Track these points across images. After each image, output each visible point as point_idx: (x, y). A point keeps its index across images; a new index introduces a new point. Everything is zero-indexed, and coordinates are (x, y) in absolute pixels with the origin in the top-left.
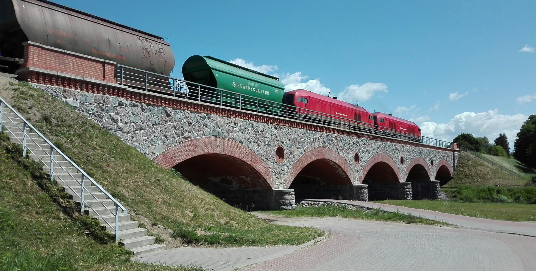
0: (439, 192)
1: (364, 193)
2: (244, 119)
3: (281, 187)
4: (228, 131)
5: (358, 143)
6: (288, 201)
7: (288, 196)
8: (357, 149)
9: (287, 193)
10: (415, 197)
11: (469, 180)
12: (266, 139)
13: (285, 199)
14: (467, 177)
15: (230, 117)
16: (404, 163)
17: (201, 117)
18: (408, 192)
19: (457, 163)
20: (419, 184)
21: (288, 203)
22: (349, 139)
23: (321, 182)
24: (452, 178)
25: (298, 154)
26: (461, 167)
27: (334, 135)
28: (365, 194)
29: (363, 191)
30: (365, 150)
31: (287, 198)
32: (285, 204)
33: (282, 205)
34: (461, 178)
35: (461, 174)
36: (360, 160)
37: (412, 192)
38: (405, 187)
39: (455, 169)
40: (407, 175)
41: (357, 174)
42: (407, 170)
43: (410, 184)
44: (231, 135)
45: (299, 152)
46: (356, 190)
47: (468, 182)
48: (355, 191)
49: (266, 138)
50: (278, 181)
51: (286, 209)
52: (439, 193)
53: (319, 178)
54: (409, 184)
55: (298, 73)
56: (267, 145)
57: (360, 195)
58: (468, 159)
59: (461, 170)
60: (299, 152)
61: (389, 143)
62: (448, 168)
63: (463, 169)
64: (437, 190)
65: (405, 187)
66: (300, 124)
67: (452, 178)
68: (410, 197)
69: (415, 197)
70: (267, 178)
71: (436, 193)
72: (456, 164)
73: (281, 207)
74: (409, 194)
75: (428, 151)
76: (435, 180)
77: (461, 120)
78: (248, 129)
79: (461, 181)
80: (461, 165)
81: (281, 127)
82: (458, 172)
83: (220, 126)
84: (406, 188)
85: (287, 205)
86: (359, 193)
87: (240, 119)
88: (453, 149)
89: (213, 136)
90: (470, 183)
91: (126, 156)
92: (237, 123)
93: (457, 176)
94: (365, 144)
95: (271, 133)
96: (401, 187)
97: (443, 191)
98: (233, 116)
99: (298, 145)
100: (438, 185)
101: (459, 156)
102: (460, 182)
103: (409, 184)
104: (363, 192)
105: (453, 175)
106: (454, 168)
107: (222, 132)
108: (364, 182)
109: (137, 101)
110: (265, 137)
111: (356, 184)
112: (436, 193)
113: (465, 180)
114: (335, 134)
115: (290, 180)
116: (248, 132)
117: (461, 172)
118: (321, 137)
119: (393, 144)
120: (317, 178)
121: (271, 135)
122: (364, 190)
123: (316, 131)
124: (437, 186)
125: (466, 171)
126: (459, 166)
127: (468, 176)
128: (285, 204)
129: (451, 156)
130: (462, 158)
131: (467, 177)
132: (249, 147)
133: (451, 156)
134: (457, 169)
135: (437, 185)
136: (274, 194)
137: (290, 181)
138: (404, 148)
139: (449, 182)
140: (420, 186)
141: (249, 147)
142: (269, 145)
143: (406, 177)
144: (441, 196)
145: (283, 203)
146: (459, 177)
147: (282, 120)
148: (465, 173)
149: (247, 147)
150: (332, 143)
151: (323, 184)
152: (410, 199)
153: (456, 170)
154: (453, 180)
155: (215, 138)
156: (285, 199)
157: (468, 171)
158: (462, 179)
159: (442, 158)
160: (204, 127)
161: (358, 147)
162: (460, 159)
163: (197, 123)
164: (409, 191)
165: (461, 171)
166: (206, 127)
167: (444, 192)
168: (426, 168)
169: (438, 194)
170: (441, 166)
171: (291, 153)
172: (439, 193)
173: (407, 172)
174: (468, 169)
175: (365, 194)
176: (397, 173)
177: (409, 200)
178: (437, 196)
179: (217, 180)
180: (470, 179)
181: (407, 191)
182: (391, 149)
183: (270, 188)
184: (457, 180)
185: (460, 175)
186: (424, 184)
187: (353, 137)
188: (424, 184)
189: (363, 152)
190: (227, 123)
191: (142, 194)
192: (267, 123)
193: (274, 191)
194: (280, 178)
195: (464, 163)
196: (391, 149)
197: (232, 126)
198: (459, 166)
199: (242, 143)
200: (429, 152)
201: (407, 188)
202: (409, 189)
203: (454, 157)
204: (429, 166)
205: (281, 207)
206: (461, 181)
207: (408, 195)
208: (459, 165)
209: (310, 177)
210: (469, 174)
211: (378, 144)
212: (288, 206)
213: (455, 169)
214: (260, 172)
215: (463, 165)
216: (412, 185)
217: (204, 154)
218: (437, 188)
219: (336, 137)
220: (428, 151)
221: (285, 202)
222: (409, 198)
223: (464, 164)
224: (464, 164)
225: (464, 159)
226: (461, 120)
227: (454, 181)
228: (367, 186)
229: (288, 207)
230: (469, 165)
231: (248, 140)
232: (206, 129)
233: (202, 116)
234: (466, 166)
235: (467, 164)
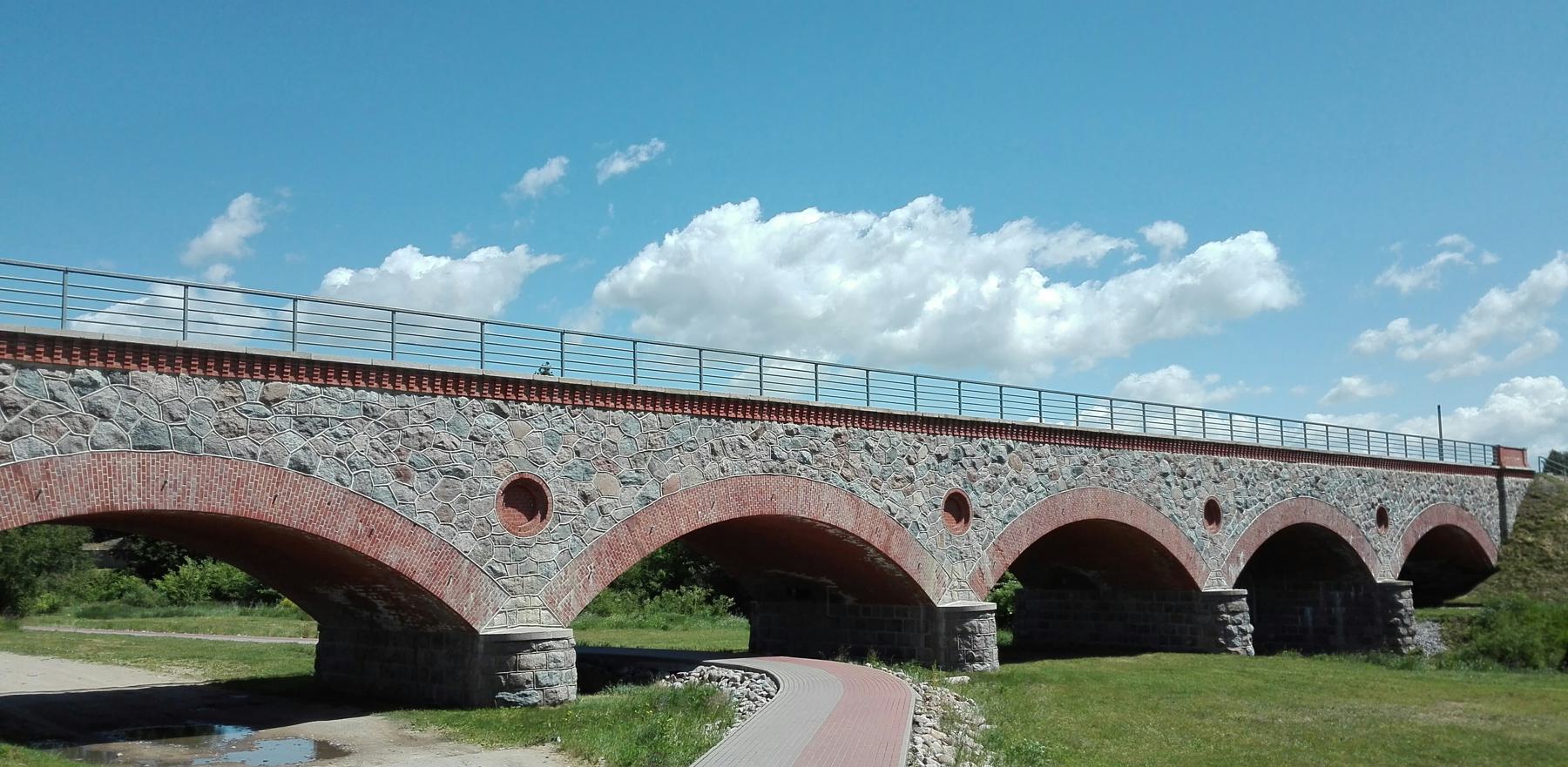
0: (1407, 621)
1: (974, 633)
2: (795, 423)
3: (527, 621)
4: (223, 427)
5: (965, 455)
6: (528, 675)
7: (528, 656)
8: (959, 478)
9: (1399, 588)
10: (1266, 645)
11: (1555, 575)
12: (440, 454)
13: (517, 667)
14: (1546, 565)
15: (238, 380)
16: (1223, 521)
17: (73, 384)
18: (1230, 627)
19: (1518, 516)
21: (528, 682)
22: (914, 442)
23: (840, 592)
24: (1496, 570)
25: (1411, 514)
26: (1531, 530)
27: (828, 432)
28: (977, 638)
29: (972, 626)
30: (1004, 480)
31: (524, 664)
32: (515, 686)
33: (503, 689)
34: (1526, 571)
35: (1526, 555)
36: (976, 516)
37: (1252, 622)
38: (1222, 607)
39: (1509, 537)
40: (1243, 565)
41: (959, 566)
42: (1241, 545)
43: (1244, 596)
44: (244, 442)
45: (631, 495)
46: (944, 624)
47: (1549, 586)
48: (942, 629)
49: (443, 448)
50: (508, 602)
51: (516, 704)
52: (1406, 626)
53: (830, 581)
54: (1240, 597)
56: (447, 473)
57: (958, 640)
58: (1560, 503)
59: (1530, 539)
60: (631, 495)
61: (1138, 454)
62: (1474, 536)
63: (1537, 536)
64: (1401, 616)
65: (1222, 607)
66: (1034, 431)
67: (1496, 570)
68: (1244, 645)
69: (1266, 645)
70: (450, 596)
71: (1396, 625)
72: (1511, 521)
73: (500, 695)
74: (1236, 632)
76: (1399, 579)
78: (341, 420)
79: (1525, 581)
80: (1532, 523)
81: (533, 407)
82: (1516, 548)
83: (177, 412)
84: (1223, 609)
85: (524, 688)
86: (956, 633)
87: (294, 386)
88: (1498, 467)
89: (144, 447)
90: (1556, 589)
92: (277, 400)
93: (1514, 560)
94: (1001, 460)
95: (471, 429)
96: (1206, 608)
97: (1431, 616)
98: (1012, 436)
99: (625, 470)
100: (1406, 599)
101: (1530, 489)
102: (1519, 585)
103: (1240, 597)
104: (970, 630)
105: (1499, 559)
106: (1504, 533)
107: (192, 434)
108: (1404, 575)
109: (208, 374)
110: (435, 446)
111: (953, 600)
112: (1396, 625)
113: (1539, 576)
114: (832, 427)
115: (582, 594)
116: (340, 429)
117: (1526, 547)
118: (755, 439)
119: (1159, 454)
120: (824, 580)
121: (472, 438)
122: (974, 622)
123: (728, 418)
124: (1401, 601)
125: (1548, 544)
126: (1524, 526)
127: (1550, 560)
128: (515, 686)
130: (1536, 497)
131: (1546, 565)
132: (344, 485)
134: (1513, 537)
135: (1401, 597)
136: (481, 647)
137: (1236, 571)
138: (1222, 469)
139: (1481, 586)
140: (1339, 601)
141: (344, 485)
142: (460, 474)
144: (1416, 637)
145: (507, 681)
146: (1520, 565)
147: (899, 418)
148: (1541, 549)
149: (336, 483)
150: (819, 460)
151: (849, 600)
152: (1238, 649)
153: (1512, 540)
154: (1497, 575)
155: (148, 456)
156: (517, 667)
157: (1553, 545)
158: (1527, 573)
159: (1435, 500)
160: (90, 417)
161: (961, 471)
162: (1531, 500)
163: (47, 406)
164: (1234, 624)
165: (1529, 544)
166: (101, 416)
167: (1436, 621)
168: (1350, 539)
169: (1402, 630)
170: (1431, 527)
171: (585, 498)
172: (1406, 626)
174: (1556, 535)
175: (977, 638)
176: (1182, 559)
177: (1237, 653)
178: (1402, 636)
179: (338, 596)
180: (1557, 572)
181: (1226, 623)
182: (1146, 474)
183: (1190, 584)
184: (1511, 575)
185: (1525, 558)
186: (1352, 594)
187: (935, 435)
188: (1352, 594)
189: (990, 488)
190: (219, 399)
192: (452, 396)
193: (482, 639)
194: (518, 589)
195: (1543, 515)
196: (1146, 474)
197: (248, 412)
198: (1524, 526)
199: (305, 470)
200: (1364, 481)
201: (1229, 612)
202: (1234, 613)
203: (1502, 496)
205: (500, 695)
206: (1525, 581)
207: (1231, 635)
208: (1523, 523)
209: (802, 576)
210: (1557, 554)
211: (1075, 457)
212: (528, 692)
213: (1509, 537)
214: (409, 573)
215: (1538, 523)
216: (1413, 588)
217: (87, 513)
218: (1401, 606)
219: (838, 436)
221: (513, 677)
222: (1235, 646)
223: (1542, 518)
224: (1542, 518)
225: (1544, 502)
227: (1499, 579)
228: (1245, 592)
229: (526, 695)
230: (1558, 524)
231: (341, 458)
232: (97, 425)
233: (76, 378)
234: (1549, 528)
235: (1553, 521)
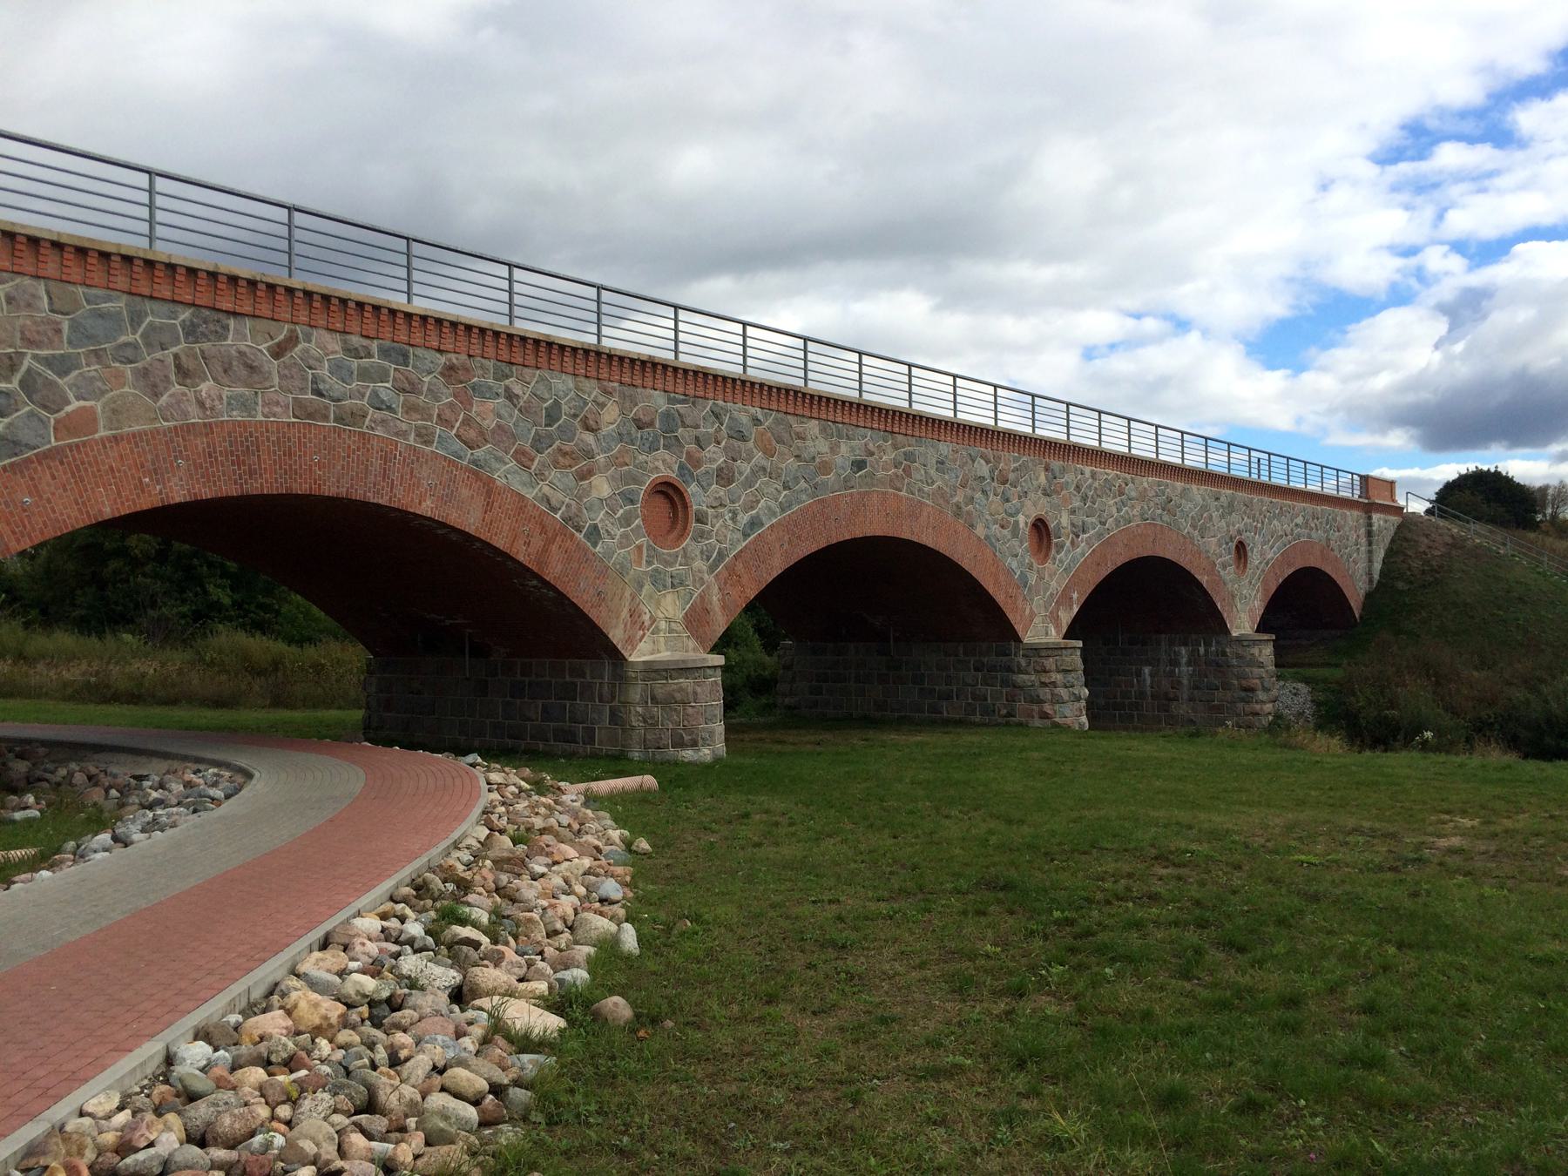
20: (1183, 650)
40: (1076, 609)
55: (301, 1145)
61: (945, 448)
75: (1217, 499)
76: (1258, 631)
77: (688, 754)
88: (1366, 501)
91: (1236, 1043)
119: (974, 451)
129: (1356, 529)
133: (1356, 529)
140: (1184, 660)
143: (1066, 617)
173: (1075, 596)
186: (1202, 650)
191: (1502, 937)
204: (1224, 567)
220: (1217, 499)
226: (688, 754)
